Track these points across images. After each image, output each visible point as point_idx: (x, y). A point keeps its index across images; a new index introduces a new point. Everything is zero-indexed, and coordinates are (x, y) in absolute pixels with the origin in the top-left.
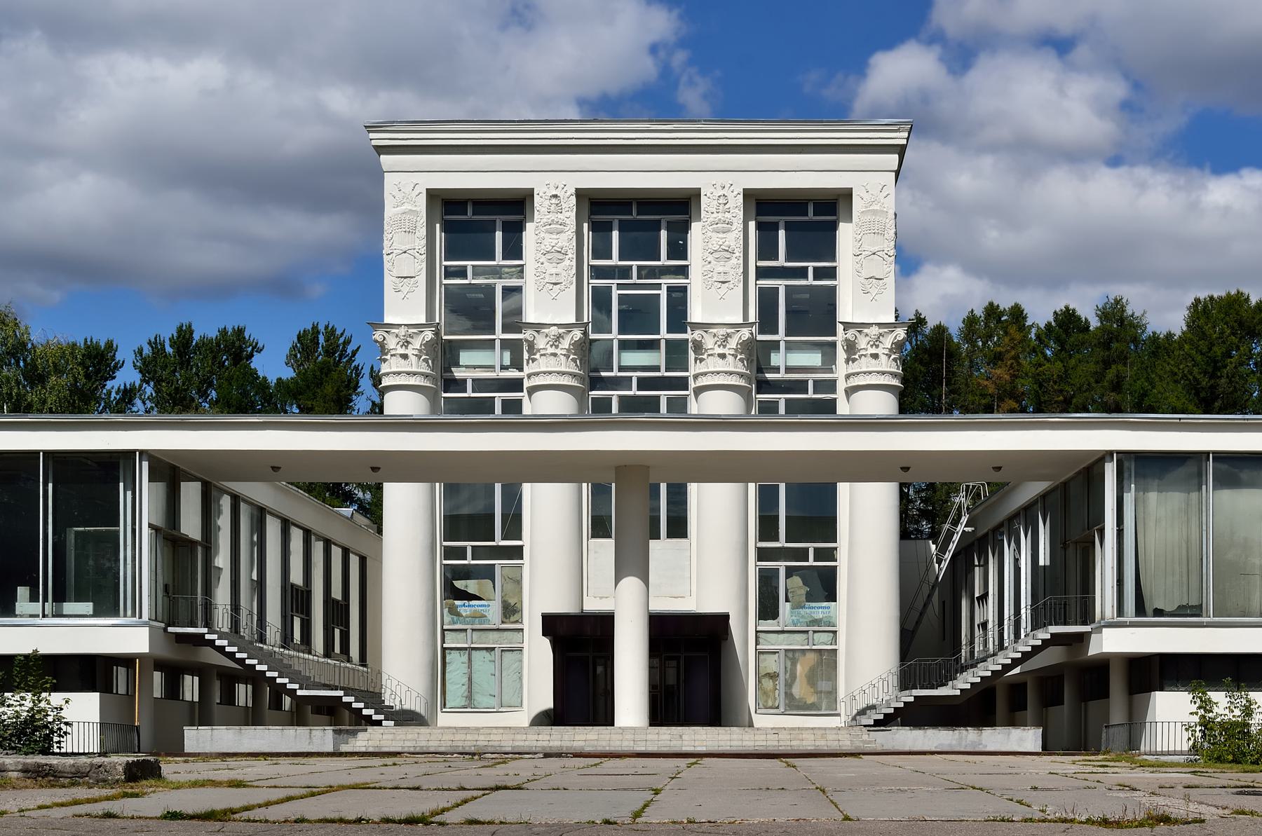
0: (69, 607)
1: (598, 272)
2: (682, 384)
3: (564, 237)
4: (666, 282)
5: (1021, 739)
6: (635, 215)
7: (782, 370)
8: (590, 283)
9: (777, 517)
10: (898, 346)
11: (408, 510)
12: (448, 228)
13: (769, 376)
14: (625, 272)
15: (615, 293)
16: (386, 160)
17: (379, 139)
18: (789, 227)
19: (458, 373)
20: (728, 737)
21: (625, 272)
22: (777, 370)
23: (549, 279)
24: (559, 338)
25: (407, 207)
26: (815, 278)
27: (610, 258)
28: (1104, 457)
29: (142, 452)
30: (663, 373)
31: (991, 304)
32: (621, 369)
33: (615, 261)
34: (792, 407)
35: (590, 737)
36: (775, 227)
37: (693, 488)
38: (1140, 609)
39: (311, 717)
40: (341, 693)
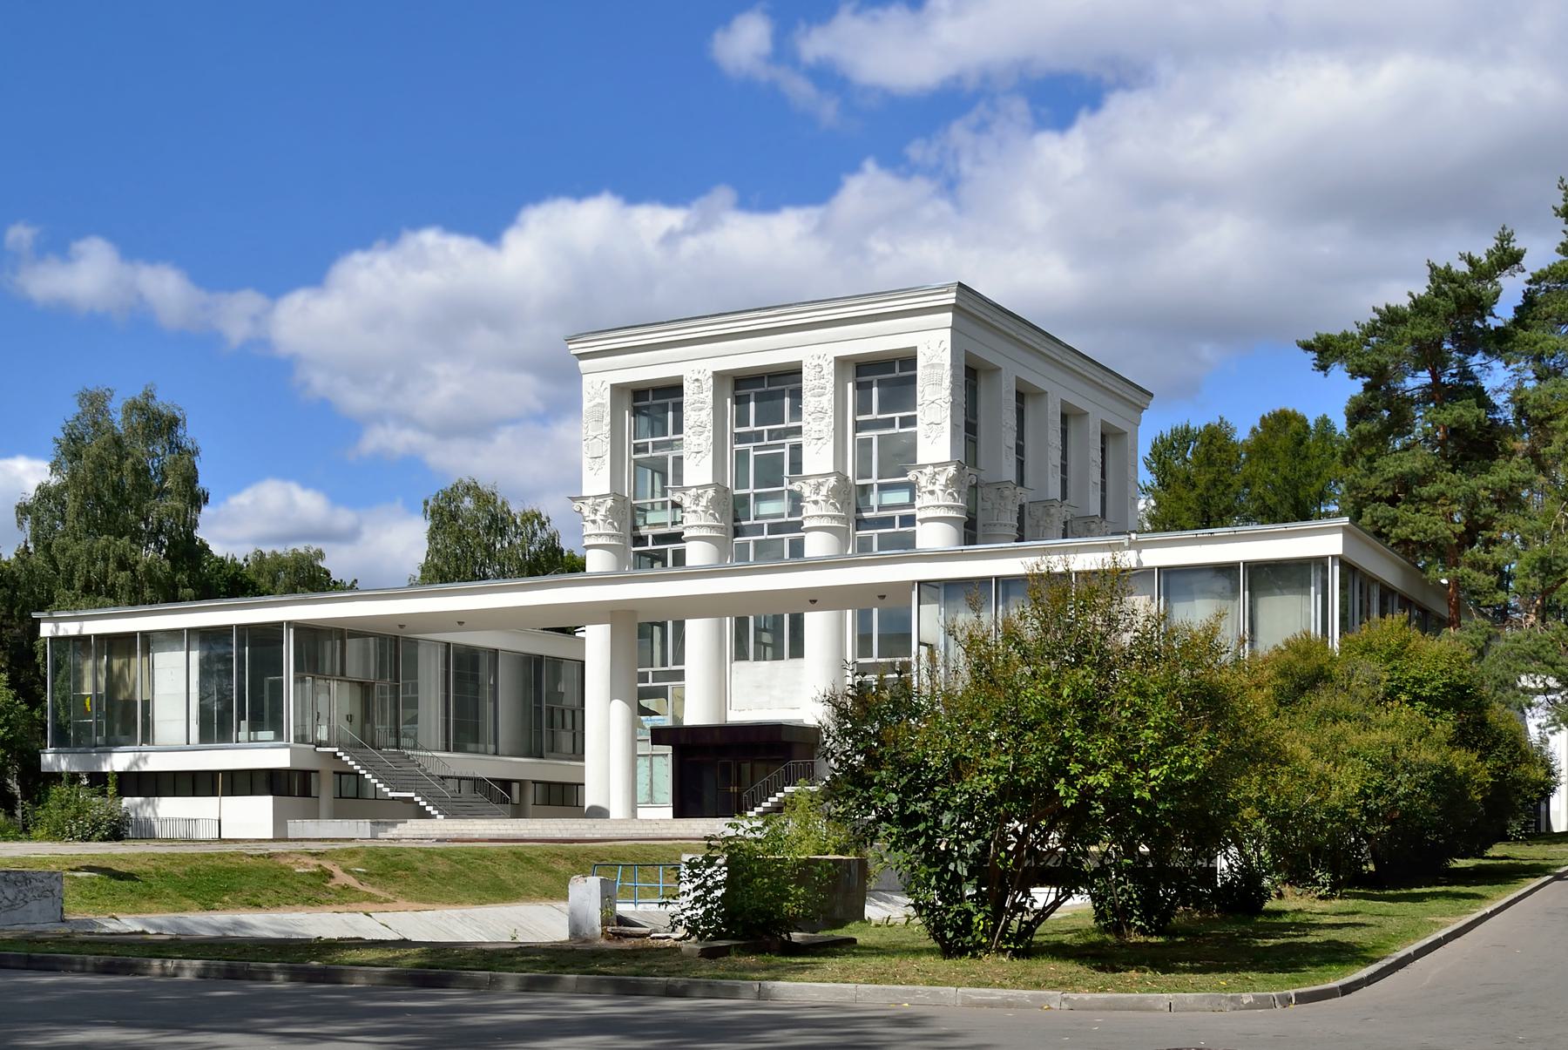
0: (262, 735)
1: (740, 438)
2: (797, 526)
3: (704, 413)
6: (766, 388)
8: (731, 448)
9: (910, 635)
10: (953, 481)
11: (596, 643)
12: (636, 412)
13: (866, 515)
15: (752, 454)
16: (583, 365)
17: (576, 348)
18: (880, 383)
19: (643, 531)
21: (758, 436)
22: (871, 509)
23: (820, 438)
24: (819, 485)
25: (598, 400)
26: (901, 426)
28: (908, 585)
29: (289, 623)
30: (786, 519)
33: (752, 427)
34: (885, 543)
36: (869, 385)
37: (688, 623)
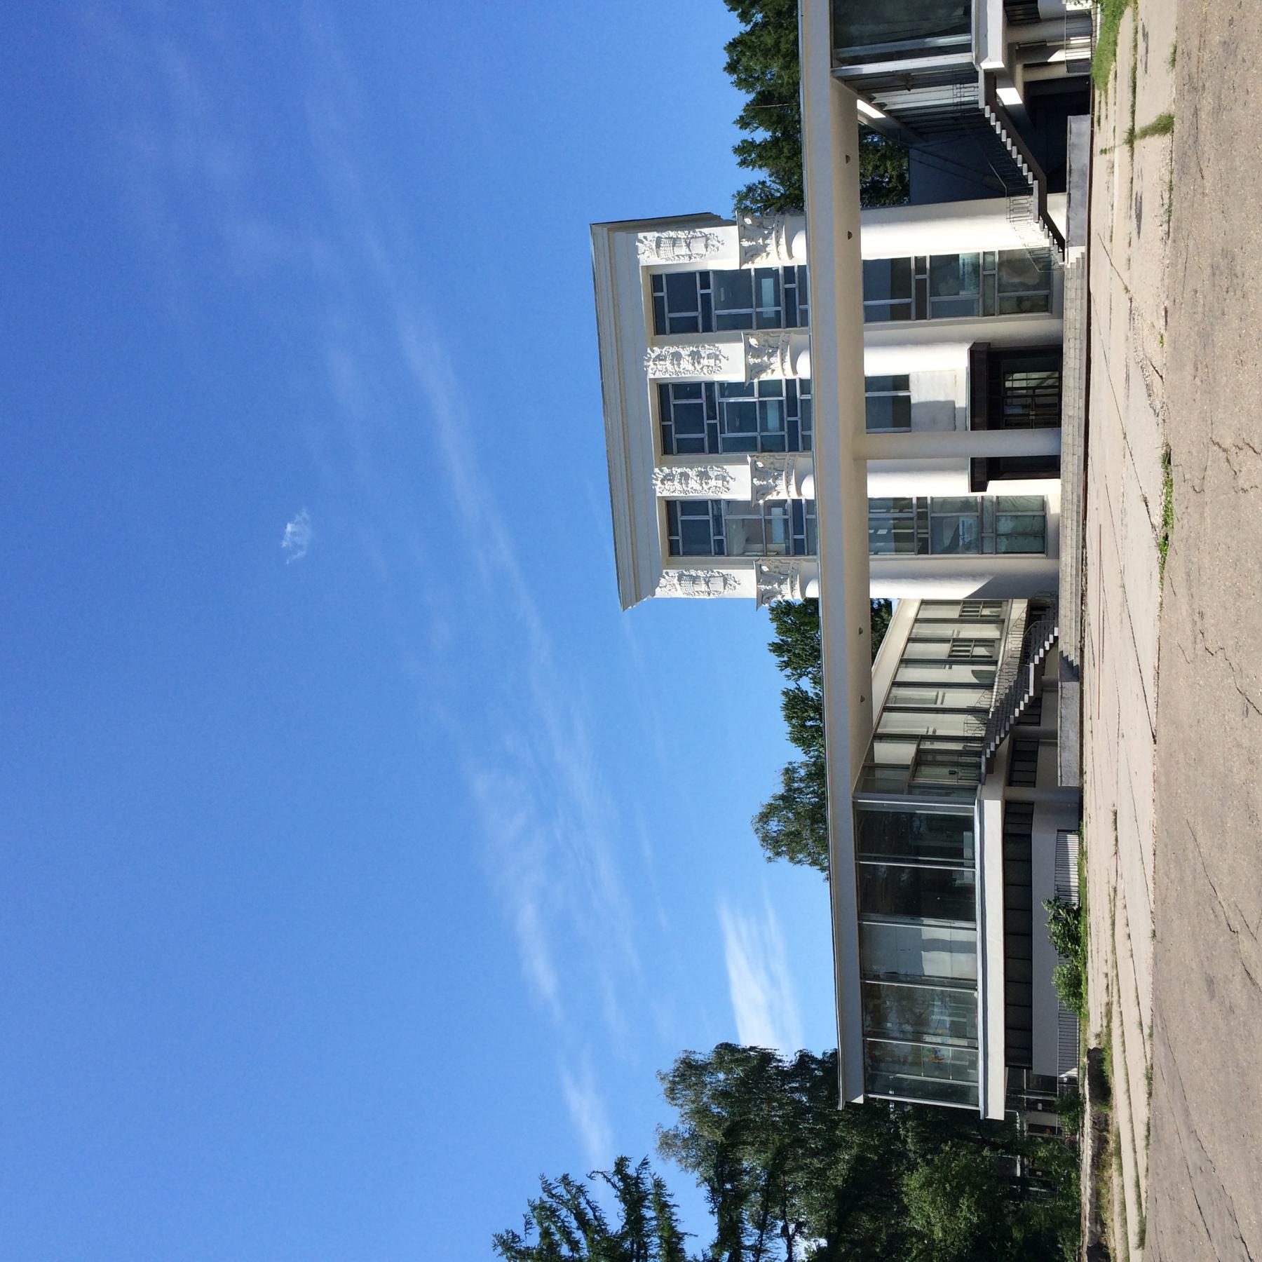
4: (718, 399)
5: (1079, 135)
7: (778, 308)
14: (713, 428)
20: (1072, 351)
21: (713, 428)
27: (703, 439)
31: (725, 69)
32: (782, 429)
35: (1072, 355)
38: (966, 29)
39: (1044, 727)
40: (1032, 666)
